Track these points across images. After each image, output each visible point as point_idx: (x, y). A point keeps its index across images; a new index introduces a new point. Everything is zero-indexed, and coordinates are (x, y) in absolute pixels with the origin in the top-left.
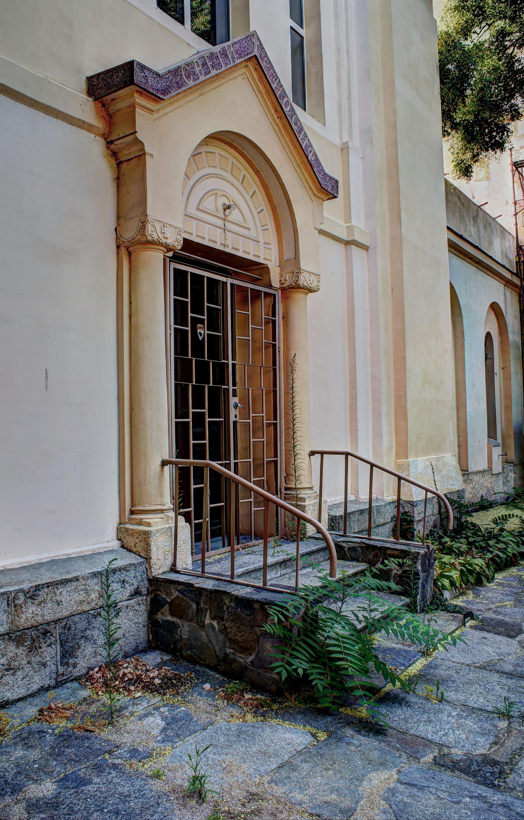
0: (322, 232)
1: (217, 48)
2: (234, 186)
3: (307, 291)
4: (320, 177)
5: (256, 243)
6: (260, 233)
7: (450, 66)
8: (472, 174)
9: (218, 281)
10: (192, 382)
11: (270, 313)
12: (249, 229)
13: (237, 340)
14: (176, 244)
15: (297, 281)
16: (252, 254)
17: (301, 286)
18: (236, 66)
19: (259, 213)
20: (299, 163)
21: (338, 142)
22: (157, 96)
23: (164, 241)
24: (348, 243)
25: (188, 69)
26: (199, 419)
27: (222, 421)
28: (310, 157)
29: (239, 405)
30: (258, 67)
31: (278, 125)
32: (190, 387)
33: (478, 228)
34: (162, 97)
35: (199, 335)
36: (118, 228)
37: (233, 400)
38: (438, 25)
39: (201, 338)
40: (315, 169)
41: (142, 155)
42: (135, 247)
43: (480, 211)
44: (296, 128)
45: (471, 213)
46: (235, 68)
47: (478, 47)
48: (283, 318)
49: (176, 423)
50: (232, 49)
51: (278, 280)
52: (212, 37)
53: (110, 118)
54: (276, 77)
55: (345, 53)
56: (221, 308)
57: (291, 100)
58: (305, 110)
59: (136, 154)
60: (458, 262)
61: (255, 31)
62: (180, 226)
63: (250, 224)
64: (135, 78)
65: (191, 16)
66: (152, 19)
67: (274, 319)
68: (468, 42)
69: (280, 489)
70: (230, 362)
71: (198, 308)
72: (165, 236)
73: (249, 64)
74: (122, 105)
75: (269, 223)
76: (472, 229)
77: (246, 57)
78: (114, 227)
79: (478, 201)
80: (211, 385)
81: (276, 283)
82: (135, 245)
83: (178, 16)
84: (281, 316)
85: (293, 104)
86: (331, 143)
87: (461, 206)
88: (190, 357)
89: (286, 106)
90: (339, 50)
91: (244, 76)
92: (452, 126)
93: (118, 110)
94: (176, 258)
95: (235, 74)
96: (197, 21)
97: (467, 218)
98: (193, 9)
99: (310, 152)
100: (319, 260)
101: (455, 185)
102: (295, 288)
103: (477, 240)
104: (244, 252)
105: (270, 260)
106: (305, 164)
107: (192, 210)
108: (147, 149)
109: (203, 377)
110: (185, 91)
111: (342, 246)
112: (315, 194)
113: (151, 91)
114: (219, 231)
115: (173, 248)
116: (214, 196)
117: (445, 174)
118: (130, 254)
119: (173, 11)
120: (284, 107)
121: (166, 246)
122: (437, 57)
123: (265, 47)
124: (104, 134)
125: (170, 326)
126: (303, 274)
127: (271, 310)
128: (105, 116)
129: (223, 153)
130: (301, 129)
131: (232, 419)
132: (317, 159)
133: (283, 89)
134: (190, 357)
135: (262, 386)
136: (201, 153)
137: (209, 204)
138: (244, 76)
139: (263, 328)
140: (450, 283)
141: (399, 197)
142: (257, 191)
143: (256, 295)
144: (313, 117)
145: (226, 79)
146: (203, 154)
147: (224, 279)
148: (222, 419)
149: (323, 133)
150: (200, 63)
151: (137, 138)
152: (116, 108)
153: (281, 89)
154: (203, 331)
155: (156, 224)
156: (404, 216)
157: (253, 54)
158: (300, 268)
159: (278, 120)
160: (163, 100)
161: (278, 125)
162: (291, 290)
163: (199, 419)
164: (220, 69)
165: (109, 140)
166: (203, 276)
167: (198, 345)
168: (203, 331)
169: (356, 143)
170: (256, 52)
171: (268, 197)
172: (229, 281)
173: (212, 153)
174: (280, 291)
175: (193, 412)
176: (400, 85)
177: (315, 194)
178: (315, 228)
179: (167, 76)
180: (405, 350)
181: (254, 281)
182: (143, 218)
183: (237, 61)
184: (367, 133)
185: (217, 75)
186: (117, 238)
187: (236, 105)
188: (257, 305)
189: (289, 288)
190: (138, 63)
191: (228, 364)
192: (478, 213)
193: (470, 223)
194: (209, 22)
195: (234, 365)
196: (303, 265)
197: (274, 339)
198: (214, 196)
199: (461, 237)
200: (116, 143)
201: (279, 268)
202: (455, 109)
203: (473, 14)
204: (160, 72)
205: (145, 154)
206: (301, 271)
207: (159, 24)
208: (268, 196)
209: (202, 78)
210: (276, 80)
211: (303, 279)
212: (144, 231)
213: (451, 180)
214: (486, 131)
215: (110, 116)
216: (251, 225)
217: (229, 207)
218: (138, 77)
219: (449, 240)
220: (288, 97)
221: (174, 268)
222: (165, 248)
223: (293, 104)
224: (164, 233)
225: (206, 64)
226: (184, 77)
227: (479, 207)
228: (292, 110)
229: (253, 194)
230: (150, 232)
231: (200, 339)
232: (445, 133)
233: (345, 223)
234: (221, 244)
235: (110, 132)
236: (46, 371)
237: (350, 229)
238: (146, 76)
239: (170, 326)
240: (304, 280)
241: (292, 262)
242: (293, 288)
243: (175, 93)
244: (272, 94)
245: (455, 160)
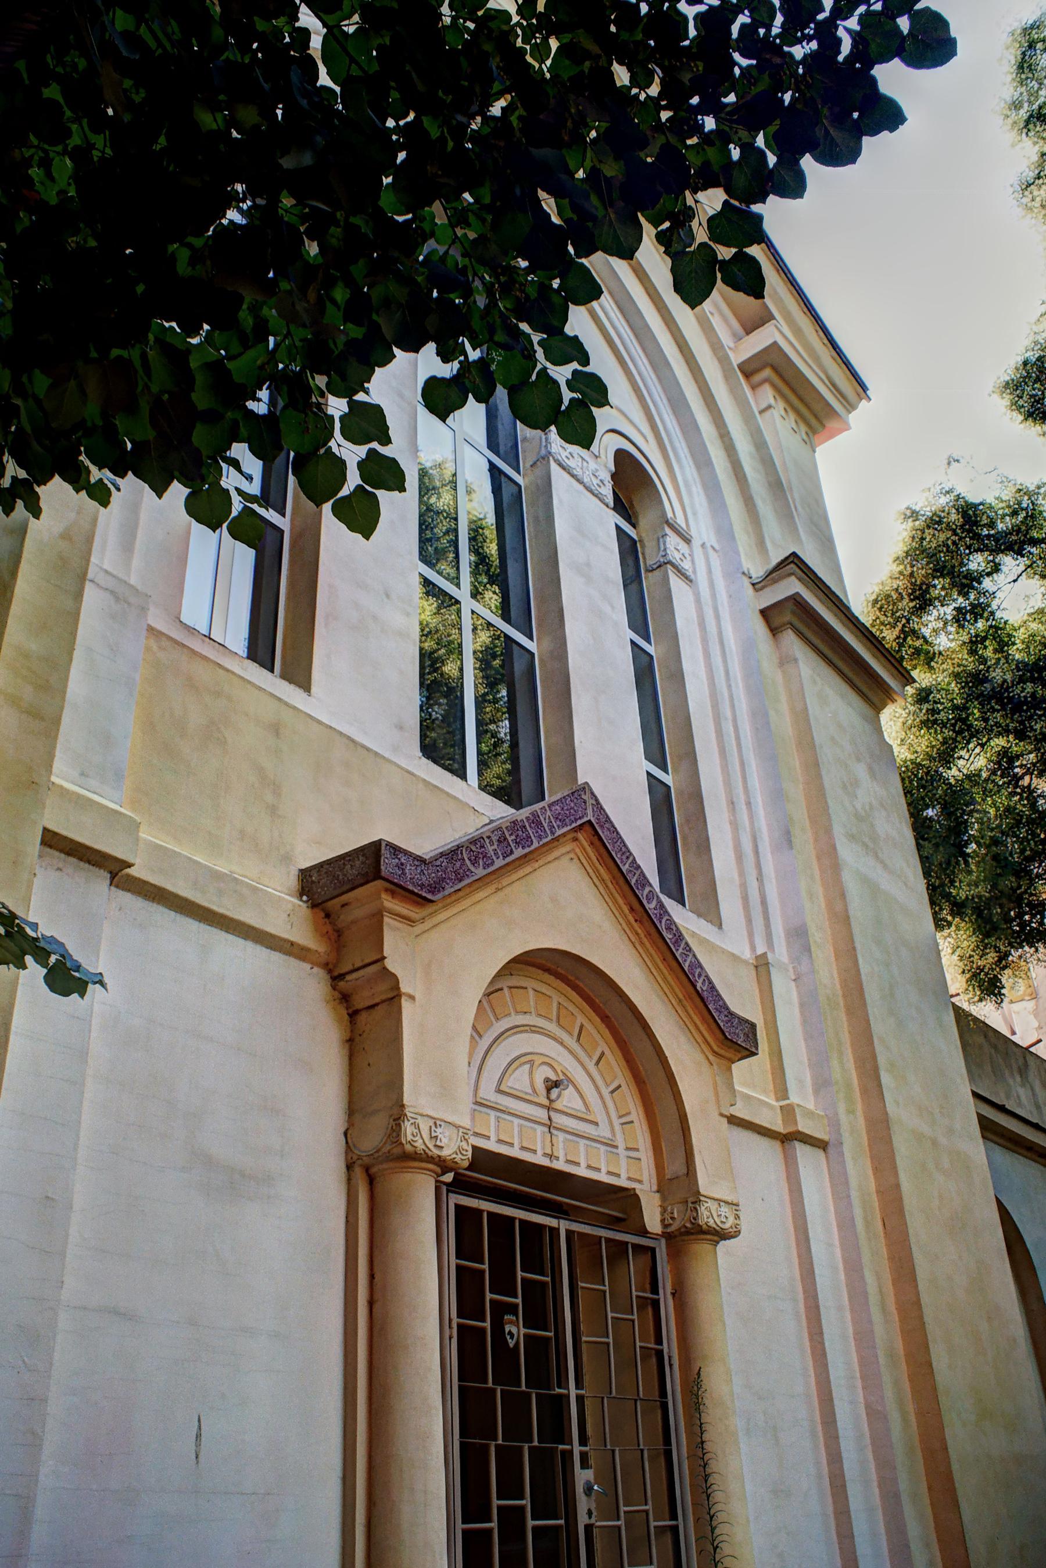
0: (734, 1121)
1: (524, 813)
2: (565, 1047)
3: (716, 1238)
5: (609, 1149)
6: (617, 1128)
7: (930, 812)
8: (1003, 991)
9: (541, 1227)
10: (496, 1439)
11: (648, 1286)
12: (596, 1124)
13: (584, 1346)
14: (458, 1158)
15: (695, 1219)
17: (704, 1227)
18: (557, 839)
19: (612, 1092)
20: (681, 996)
22: (420, 896)
23: (436, 1152)
24: (788, 1139)
25: (474, 848)
26: (512, 1519)
27: (559, 1527)
28: (699, 985)
29: (596, 1487)
30: (595, 839)
31: (637, 934)
32: (493, 1449)
33: (1032, 1089)
34: (429, 896)
35: (508, 1337)
36: (350, 1132)
37: (582, 1476)
38: (896, 754)
39: (511, 1343)
40: (711, 1007)
41: (394, 997)
42: (381, 1167)
43: (1028, 1057)
44: (670, 936)
45: (1013, 1061)
46: (556, 843)
47: (972, 778)
48: (673, 1294)
49: (464, 1531)
50: (549, 813)
52: (514, 796)
53: (339, 936)
54: (627, 853)
55: (744, 807)
56: (549, 1279)
57: (658, 890)
58: (684, 905)
59: (384, 997)
60: (1006, 1159)
61: (587, 783)
62: (466, 1122)
63: (598, 1113)
64: (383, 868)
65: (478, 765)
66: (412, 774)
67: (656, 1297)
68: (954, 772)
69: (670, 1357)
70: (573, 1392)
71: (503, 1282)
72: (438, 1143)
73: (580, 836)
74: (358, 912)
75: (631, 1106)
76: (1021, 1091)
77: (574, 825)
78: (343, 1130)
79: (1022, 1039)
80: (536, 1443)
81: (653, 1221)
82: (381, 1163)
83: (456, 766)
84: (669, 1290)
85: (661, 896)
86: (735, 958)
87: (993, 1051)
88: (490, 1384)
89: (649, 901)
90: (733, 803)
91: (572, 855)
92: (952, 910)
93: (352, 922)
94: (461, 1184)
95: (556, 853)
96: (489, 774)
97: (1007, 1073)
98: (483, 755)
99: (700, 975)
100: (736, 1178)
101: (974, 1014)
102: (692, 1234)
103: (1035, 1112)
104: (589, 1167)
105: (640, 1182)
106: (691, 998)
107: (487, 1091)
108: (404, 988)
109: (517, 1429)
110: (469, 885)
111: (777, 1144)
112: (714, 1052)
113: (411, 887)
114: (540, 1129)
115: (453, 1165)
116: (527, 1067)
117: (952, 996)
118: (371, 1180)
119: (449, 759)
120: (645, 902)
121: (442, 1163)
122: (902, 801)
123: (605, 807)
124: (327, 964)
125: (450, 1320)
126: (706, 1205)
127: (648, 1281)
128: (331, 932)
129: (544, 988)
130: (679, 937)
131: (583, 1520)
132: (712, 988)
133: (642, 872)
134: (490, 1384)
135: (641, 1393)
136: (501, 989)
137: (519, 1081)
138: (572, 855)
139: (635, 1317)
140: (999, 1202)
141: (872, 1043)
142: (607, 1052)
143: (619, 1250)
144: (699, 915)
145: (541, 862)
146: (506, 990)
147: (552, 1222)
148: (562, 1522)
149: (721, 945)
150: (495, 838)
151: (385, 968)
153: (638, 873)
154: (516, 1331)
155: (420, 1121)
156: (886, 1079)
157: (585, 819)
158: (698, 1193)
159: (636, 925)
160: (432, 901)
161: (637, 934)
162: (686, 1238)
163: (512, 1519)
164: (529, 846)
165: (336, 974)
167: (505, 1355)
168: (516, 1331)
169: (781, 953)
170: (590, 816)
172: (563, 1226)
173: (522, 988)
174: (663, 1241)
175: (499, 1507)
176: (847, 852)
177: (714, 1052)
178: (722, 1115)
179: (438, 863)
180: (927, 1348)
181: (613, 1222)
182: (395, 1111)
183: (559, 832)
184: (799, 935)
185: (525, 855)
187: (561, 906)
189: (682, 1234)
190: (389, 845)
191: (568, 1396)
192: (1026, 1062)
193: (1015, 1082)
194: (509, 773)
195: (580, 1399)
196: (705, 1183)
197: (659, 1341)
198: (527, 1067)
199: (1002, 1109)
200: (348, 978)
201: (658, 1195)
202: (952, 882)
203: (954, 731)
204: (427, 857)
205: (399, 995)
206: (702, 1198)
207: (424, 780)
208: (627, 1061)
209: (499, 863)
210: (628, 858)
211: (706, 1213)
212: (399, 1135)
213: (965, 1006)
214: (1012, 913)
215: (339, 933)
216: (600, 1116)
217: (556, 1084)
218: (388, 865)
219: (981, 1118)
220: (650, 885)
221: (456, 1205)
222: (438, 1166)
223: (661, 896)
224: (436, 1137)
225: (505, 839)
226: (468, 862)
227: (1027, 1049)
228: (661, 906)
229: (600, 1059)
230: (410, 1137)
231: (511, 1345)
232: (940, 924)
233: (777, 1100)
235: (338, 961)
236: (199, 1421)
237: (788, 1112)
238: (402, 864)
239: (450, 1320)
240: (710, 1214)
241: (680, 1183)
242: (688, 1232)
243: (453, 890)
244: (622, 881)
245: (968, 968)
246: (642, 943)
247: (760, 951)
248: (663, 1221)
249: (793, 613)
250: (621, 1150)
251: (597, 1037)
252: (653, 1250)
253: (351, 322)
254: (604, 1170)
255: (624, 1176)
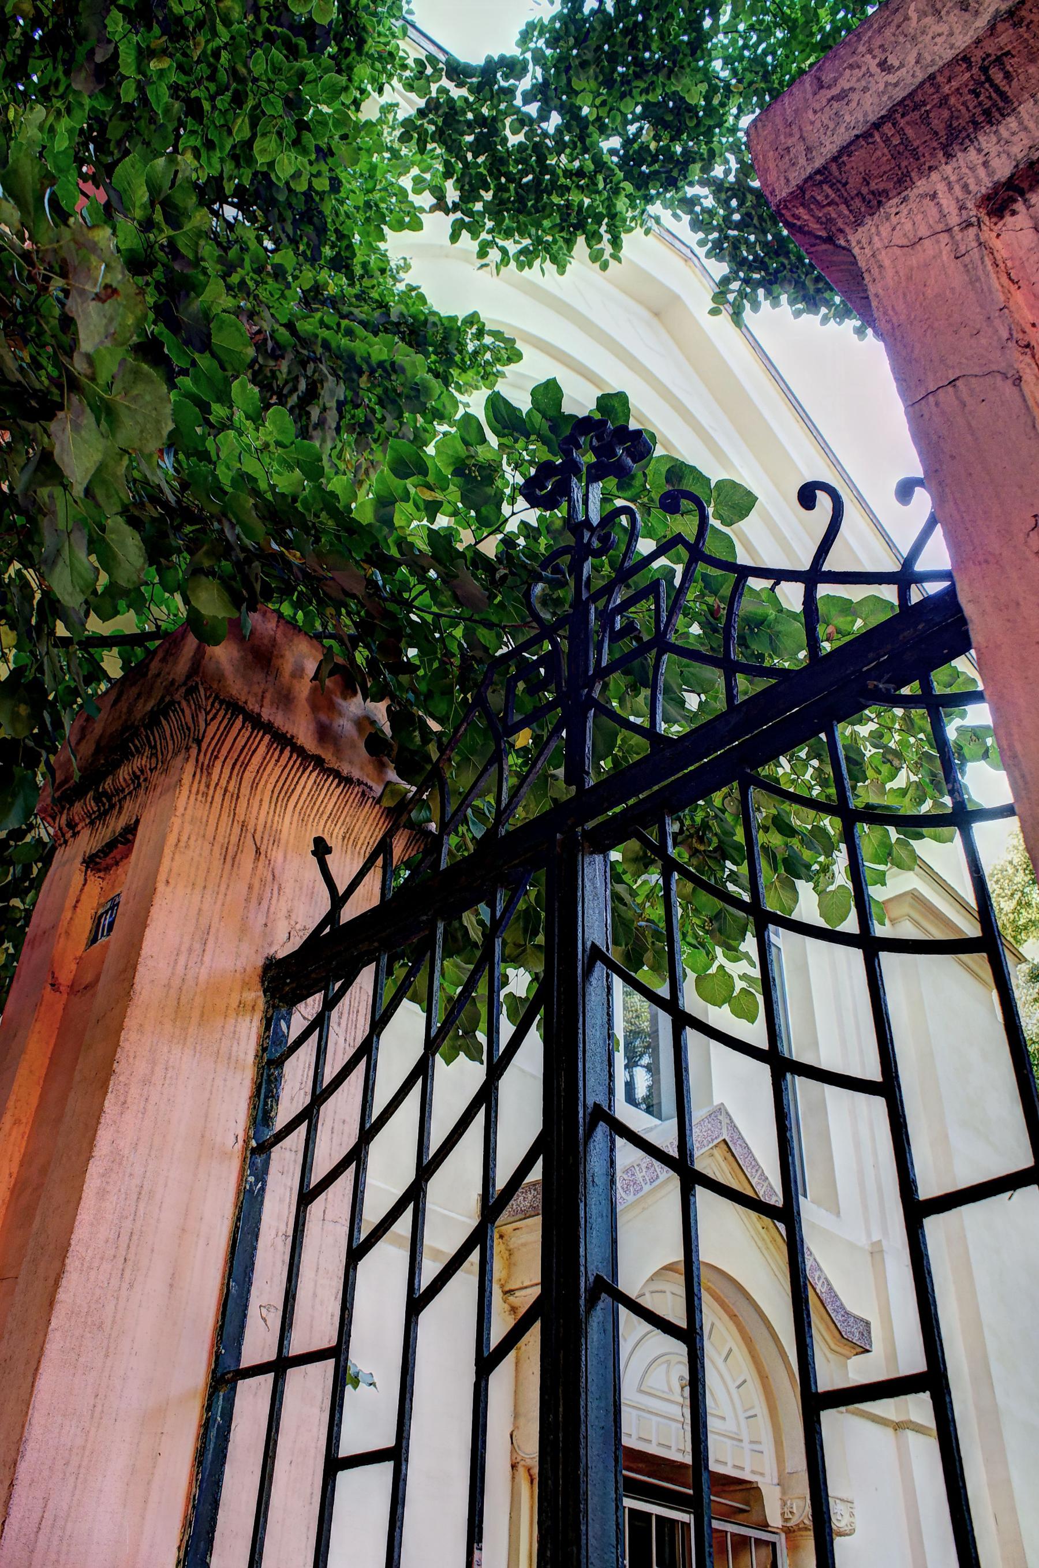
4: (838, 1318)
9: (673, 1522)
12: (724, 1418)
16: (730, 1464)
19: (739, 1387)
21: (863, 1242)
51: (779, 1511)
73: (715, 1152)
81: (775, 1520)
105: (762, 1474)
111: (890, 1431)
132: (831, 1289)
142: (735, 1349)
143: (742, 1543)
152: (520, 1242)
165: (507, 1289)
166: (650, 1515)
171: (753, 1357)
174: (783, 1536)
186: (513, 1450)
188: (745, 1560)
189: (800, 1529)
200: (517, 1293)
234: (679, 1450)
246: (768, 1248)
247: (875, 1238)
248: (783, 1514)
249: (912, 906)
250: (746, 1445)
251: (725, 1333)
252: (774, 1544)
253: (551, 810)
254: (730, 1464)
255: (748, 1469)
